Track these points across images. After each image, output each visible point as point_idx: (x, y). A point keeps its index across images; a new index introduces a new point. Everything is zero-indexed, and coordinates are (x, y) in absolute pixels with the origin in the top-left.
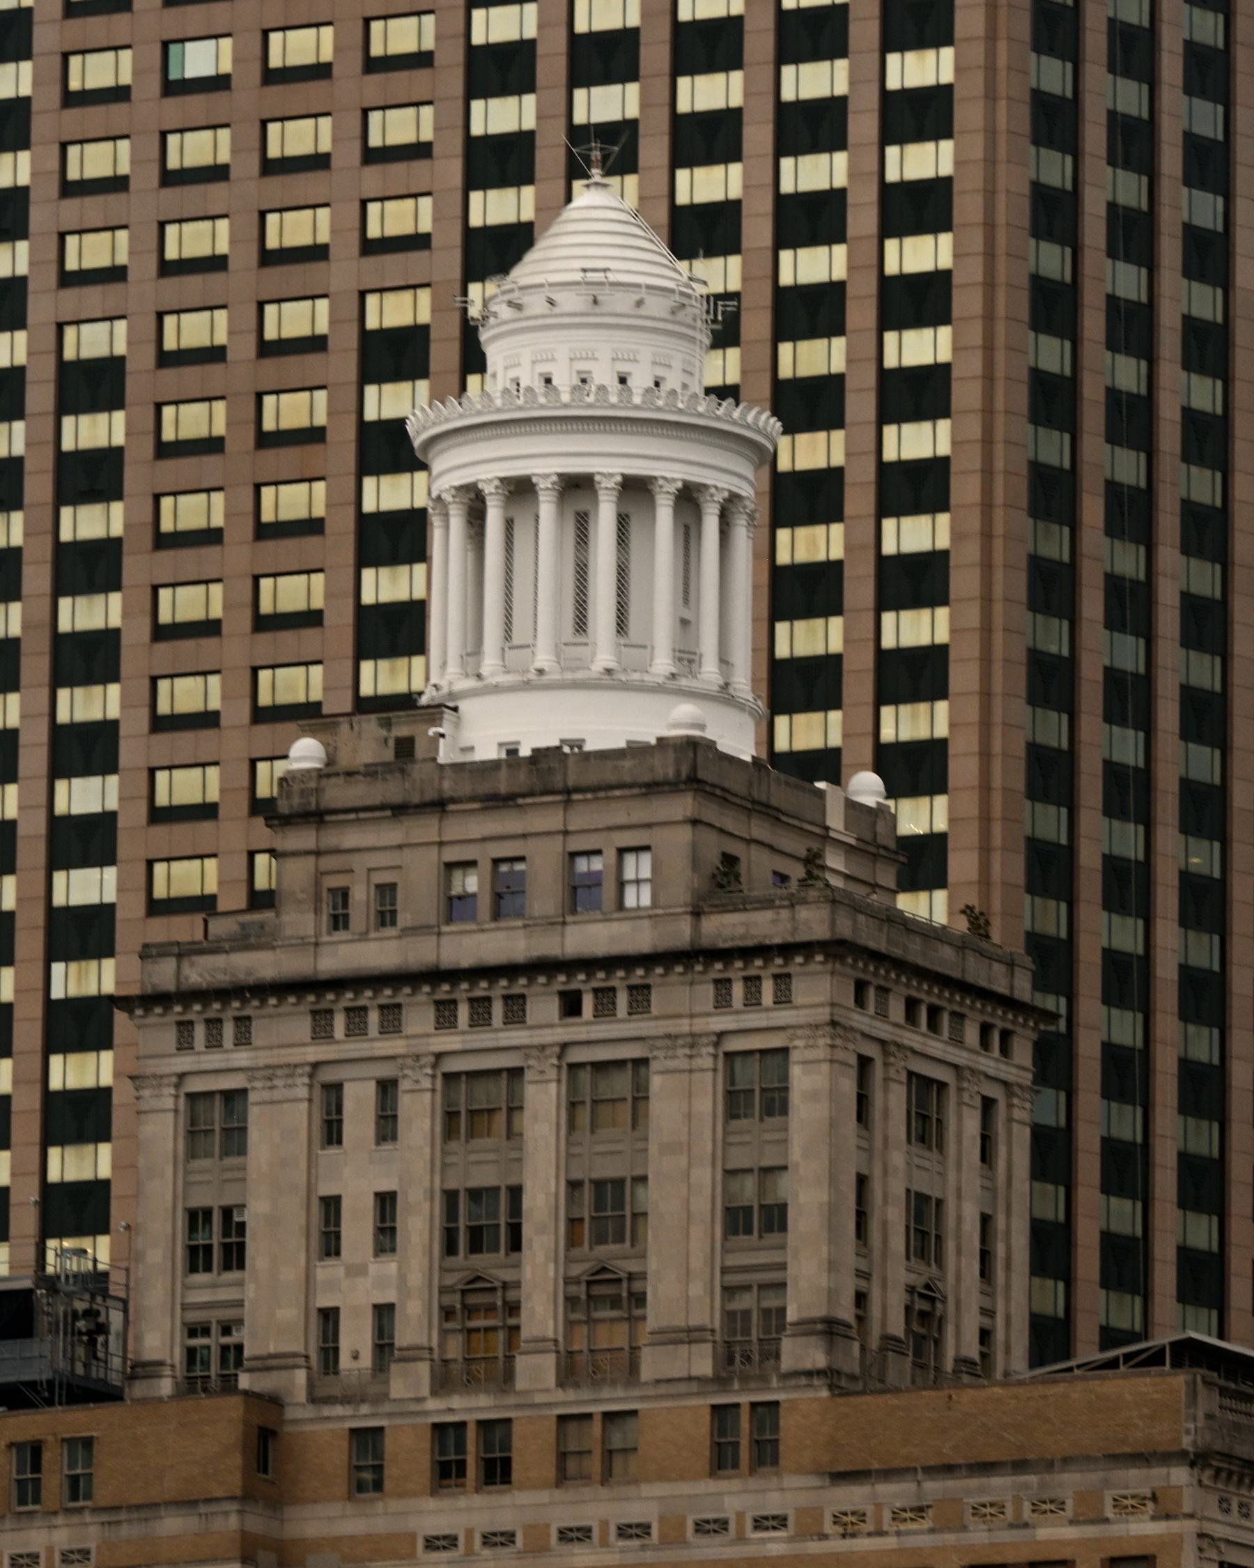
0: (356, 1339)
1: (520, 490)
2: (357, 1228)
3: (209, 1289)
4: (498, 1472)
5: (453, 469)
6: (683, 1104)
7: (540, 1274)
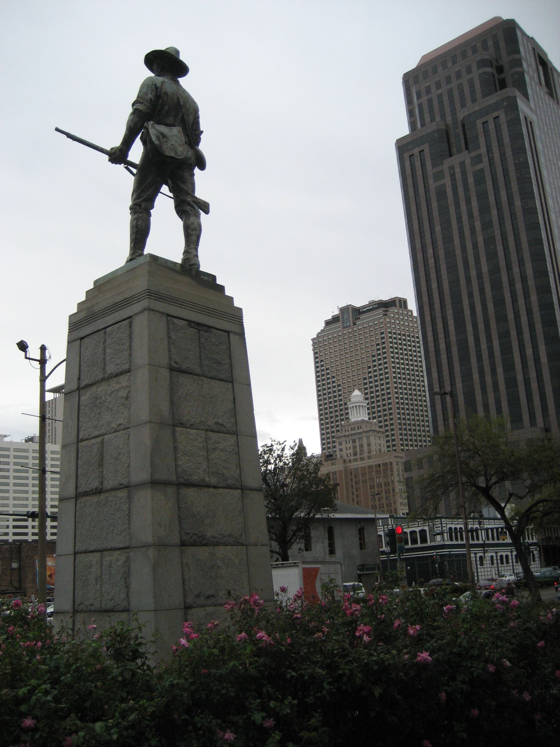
0: (349, 455)
1: (353, 407)
2: (348, 448)
3: (341, 453)
4: (363, 460)
5: (350, 406)
6: (365, 440)
7: (358, 450)
